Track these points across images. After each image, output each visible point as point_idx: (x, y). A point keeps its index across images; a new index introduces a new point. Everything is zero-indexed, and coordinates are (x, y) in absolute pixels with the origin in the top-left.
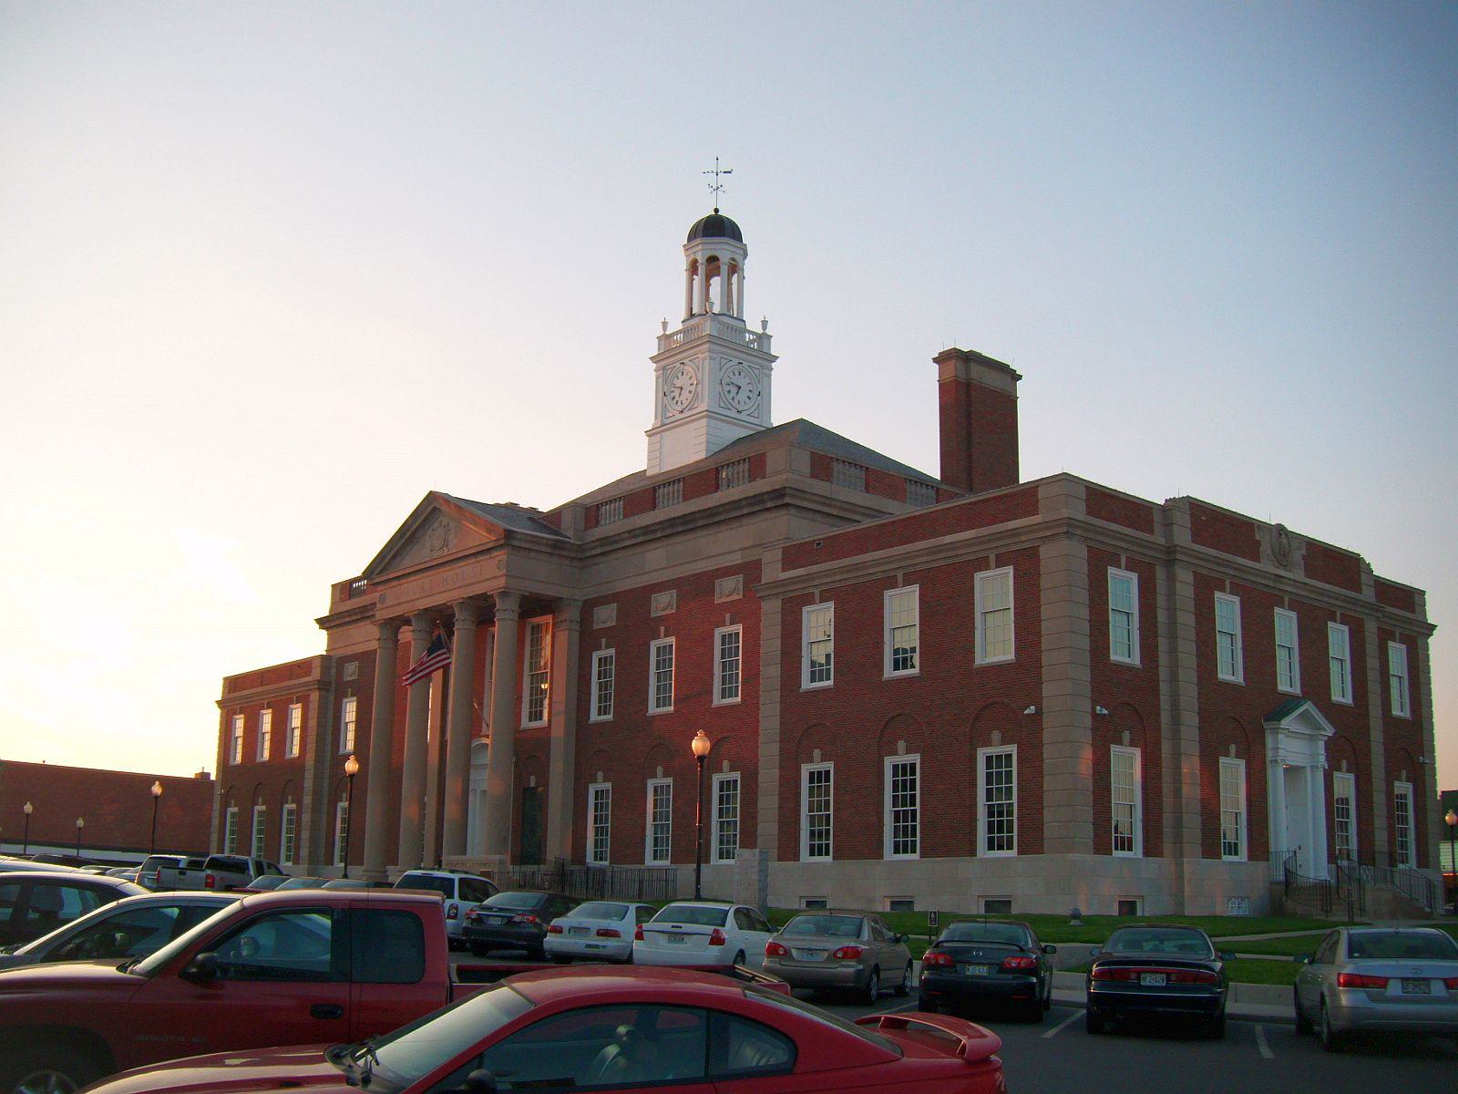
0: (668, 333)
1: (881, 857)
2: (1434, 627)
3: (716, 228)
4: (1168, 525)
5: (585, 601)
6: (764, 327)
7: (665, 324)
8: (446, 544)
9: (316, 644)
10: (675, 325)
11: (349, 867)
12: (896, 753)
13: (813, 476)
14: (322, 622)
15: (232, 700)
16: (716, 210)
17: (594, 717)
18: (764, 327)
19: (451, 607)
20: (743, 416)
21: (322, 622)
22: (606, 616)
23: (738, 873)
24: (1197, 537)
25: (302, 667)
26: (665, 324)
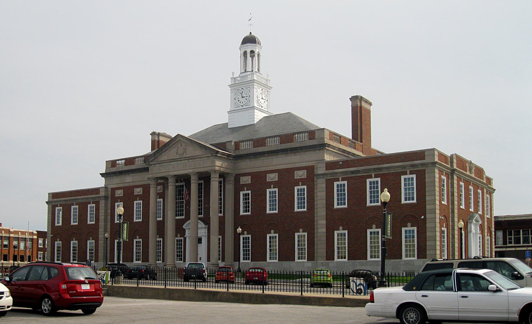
0: (235, 77)
1: (334, 260)
2: (494, 190)
3: (250, 40)
4: (452, 162)
5: (237, 175)
6: (268, 77)
7: (233, 73)
8: (185, 151)
9: (100, 182)
10: (237, 75)
11: (387, 261)
12: (372, 228)
13: (330, 139)
14: (102, 175)
15: (51, 202)
16: (251, 33)
17: (242, 213)
18: (268, 77)
19: (190, 176)
20: (263, 108)
21: (102, 175)
22: (246, 180)
23: (14, 264)
24: (330, 139)
25: (96, 191)
26: (233, 73)
